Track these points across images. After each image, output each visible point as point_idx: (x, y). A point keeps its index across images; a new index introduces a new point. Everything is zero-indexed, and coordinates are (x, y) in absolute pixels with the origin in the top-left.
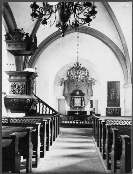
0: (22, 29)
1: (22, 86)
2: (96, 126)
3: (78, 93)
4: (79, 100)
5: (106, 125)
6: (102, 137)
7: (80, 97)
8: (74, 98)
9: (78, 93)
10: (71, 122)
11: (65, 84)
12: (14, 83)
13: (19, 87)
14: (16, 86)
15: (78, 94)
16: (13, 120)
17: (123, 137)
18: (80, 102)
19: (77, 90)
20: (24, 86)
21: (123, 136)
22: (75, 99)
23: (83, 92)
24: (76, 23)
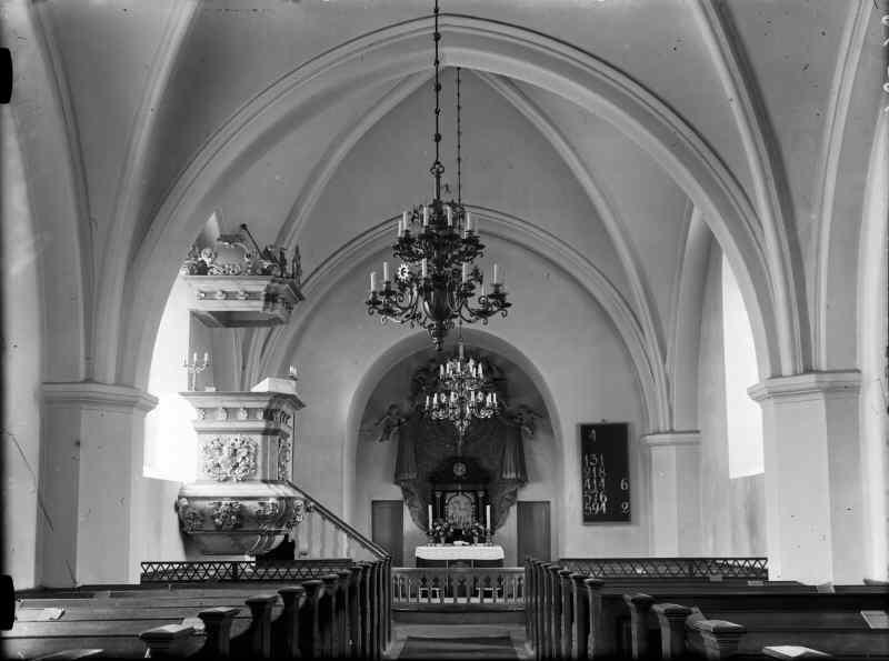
0: (244, 226)
1: (248, 447)
2: (549, 609)
3: (460, 470)
4: (466, 500)
5: (571, 575)
6: (553, 619)
7: (470, 487)
8: (444, 493)
9: (460, 470)
10: (437, 601)
11: (401, 433)
12: (214, 437)
13: (235, 450)
14: (225, 448)
15: (459, 474)
16: (171, 568)
17: (662, 610)
18: (471, 509)
19: (455, 460)
20: (253, 451)
21: (658, 608)
22: (449, 496)
23: (485, 464)
24: (439, 220)
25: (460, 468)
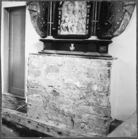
25: (36, 14)
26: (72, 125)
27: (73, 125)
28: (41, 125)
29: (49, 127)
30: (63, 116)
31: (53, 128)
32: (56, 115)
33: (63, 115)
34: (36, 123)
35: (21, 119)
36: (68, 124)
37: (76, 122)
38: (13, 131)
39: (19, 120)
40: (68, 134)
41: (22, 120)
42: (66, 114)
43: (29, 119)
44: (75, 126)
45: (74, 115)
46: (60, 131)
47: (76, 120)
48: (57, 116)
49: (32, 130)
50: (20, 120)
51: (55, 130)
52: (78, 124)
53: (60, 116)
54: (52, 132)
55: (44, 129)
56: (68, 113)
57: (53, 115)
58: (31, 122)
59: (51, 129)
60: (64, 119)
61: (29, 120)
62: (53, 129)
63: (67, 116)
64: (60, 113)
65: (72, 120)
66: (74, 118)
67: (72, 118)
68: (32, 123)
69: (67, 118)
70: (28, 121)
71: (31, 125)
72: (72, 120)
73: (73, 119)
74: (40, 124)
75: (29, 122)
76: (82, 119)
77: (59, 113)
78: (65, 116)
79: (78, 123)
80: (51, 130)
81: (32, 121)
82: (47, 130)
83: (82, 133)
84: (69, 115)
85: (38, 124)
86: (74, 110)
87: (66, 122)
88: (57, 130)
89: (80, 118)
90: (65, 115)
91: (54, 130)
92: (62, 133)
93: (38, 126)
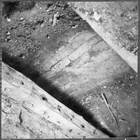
26: (22, 113)
27: (21, 113)
28: (69, 117)
29: (58, 111)
30: (34, 129)
31: (53, 108)
32: (43, 134)
33: (33, 131)
34: (74, 121)
35: (93, 133)
36: (28, 117)
37: (16, 115)
38: (100, 123)
39: (95, 133)
40: (32, 94)
41: (92, 131)
42: (29, 131)
43: (82, 129)
44: (19, 112)
45: (17, 126)
46: (44, 102)
47: (16, 118)
48: (41, 132)
49: (80, 114)
50: (94, 133)
51: (50, 106)
52: (13, 112)
53: (38, 131)
54: (55, 104)
55: (65, 112)
56: (25, 131)
57: (47, 135)
58: (81, 125)
59: (55, 108)
60: (33, 125)
61: (83, 128)
62: (53, 106)
63: (28, 128)
64: (37, 134)
65: (21, 121)
66: (18, 123)
67: (20, 123)
68: (79, 124)
69: (28, 126)
70: (84, 129)
71: (80, 121)
72: (21, 121)
73: (20, 122)
74: (69, 119)
75: (83, 127)
76: (7, 117)
77: (37, 135)
78: (31, 128)
79: (13, 114)
80: (56, 106)
81: (79, 127)
82: (61, 109)
83: (12, 90)
84: (24, 129)
85: (71, 120)
86: (14, 134)
87: (31, 120)
88: (48, 104)
89: (8, 120)
90: (30, 130)
91: (52, 105)
92: (42, 98)
93: (72, 118)
